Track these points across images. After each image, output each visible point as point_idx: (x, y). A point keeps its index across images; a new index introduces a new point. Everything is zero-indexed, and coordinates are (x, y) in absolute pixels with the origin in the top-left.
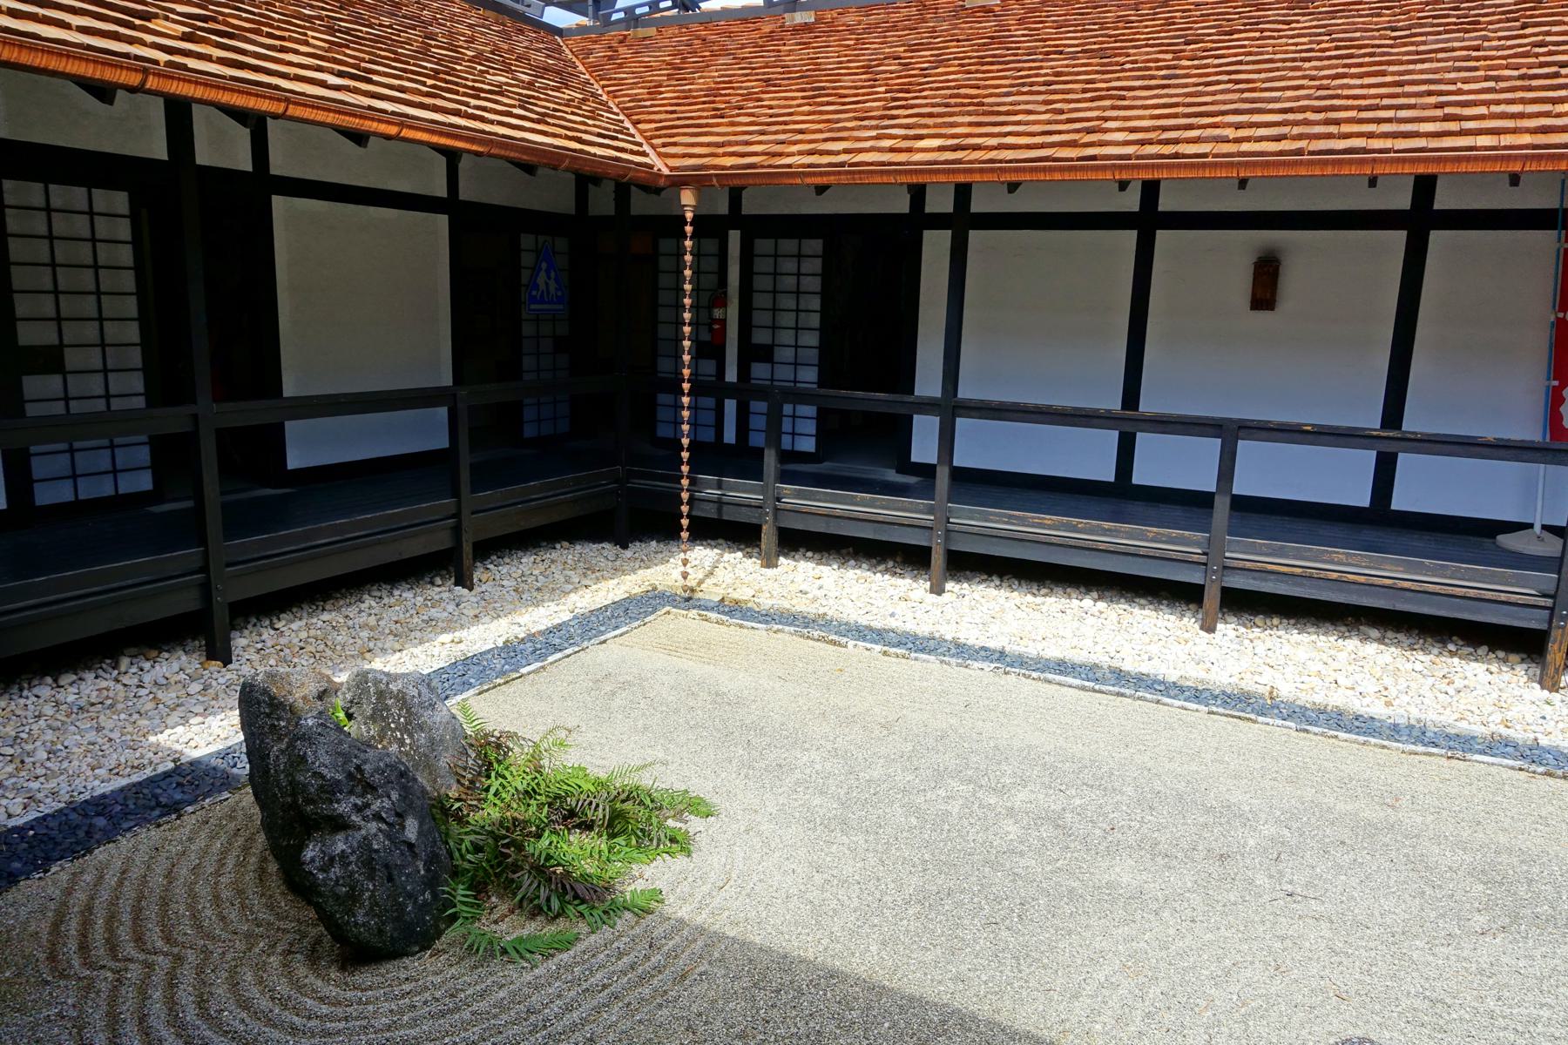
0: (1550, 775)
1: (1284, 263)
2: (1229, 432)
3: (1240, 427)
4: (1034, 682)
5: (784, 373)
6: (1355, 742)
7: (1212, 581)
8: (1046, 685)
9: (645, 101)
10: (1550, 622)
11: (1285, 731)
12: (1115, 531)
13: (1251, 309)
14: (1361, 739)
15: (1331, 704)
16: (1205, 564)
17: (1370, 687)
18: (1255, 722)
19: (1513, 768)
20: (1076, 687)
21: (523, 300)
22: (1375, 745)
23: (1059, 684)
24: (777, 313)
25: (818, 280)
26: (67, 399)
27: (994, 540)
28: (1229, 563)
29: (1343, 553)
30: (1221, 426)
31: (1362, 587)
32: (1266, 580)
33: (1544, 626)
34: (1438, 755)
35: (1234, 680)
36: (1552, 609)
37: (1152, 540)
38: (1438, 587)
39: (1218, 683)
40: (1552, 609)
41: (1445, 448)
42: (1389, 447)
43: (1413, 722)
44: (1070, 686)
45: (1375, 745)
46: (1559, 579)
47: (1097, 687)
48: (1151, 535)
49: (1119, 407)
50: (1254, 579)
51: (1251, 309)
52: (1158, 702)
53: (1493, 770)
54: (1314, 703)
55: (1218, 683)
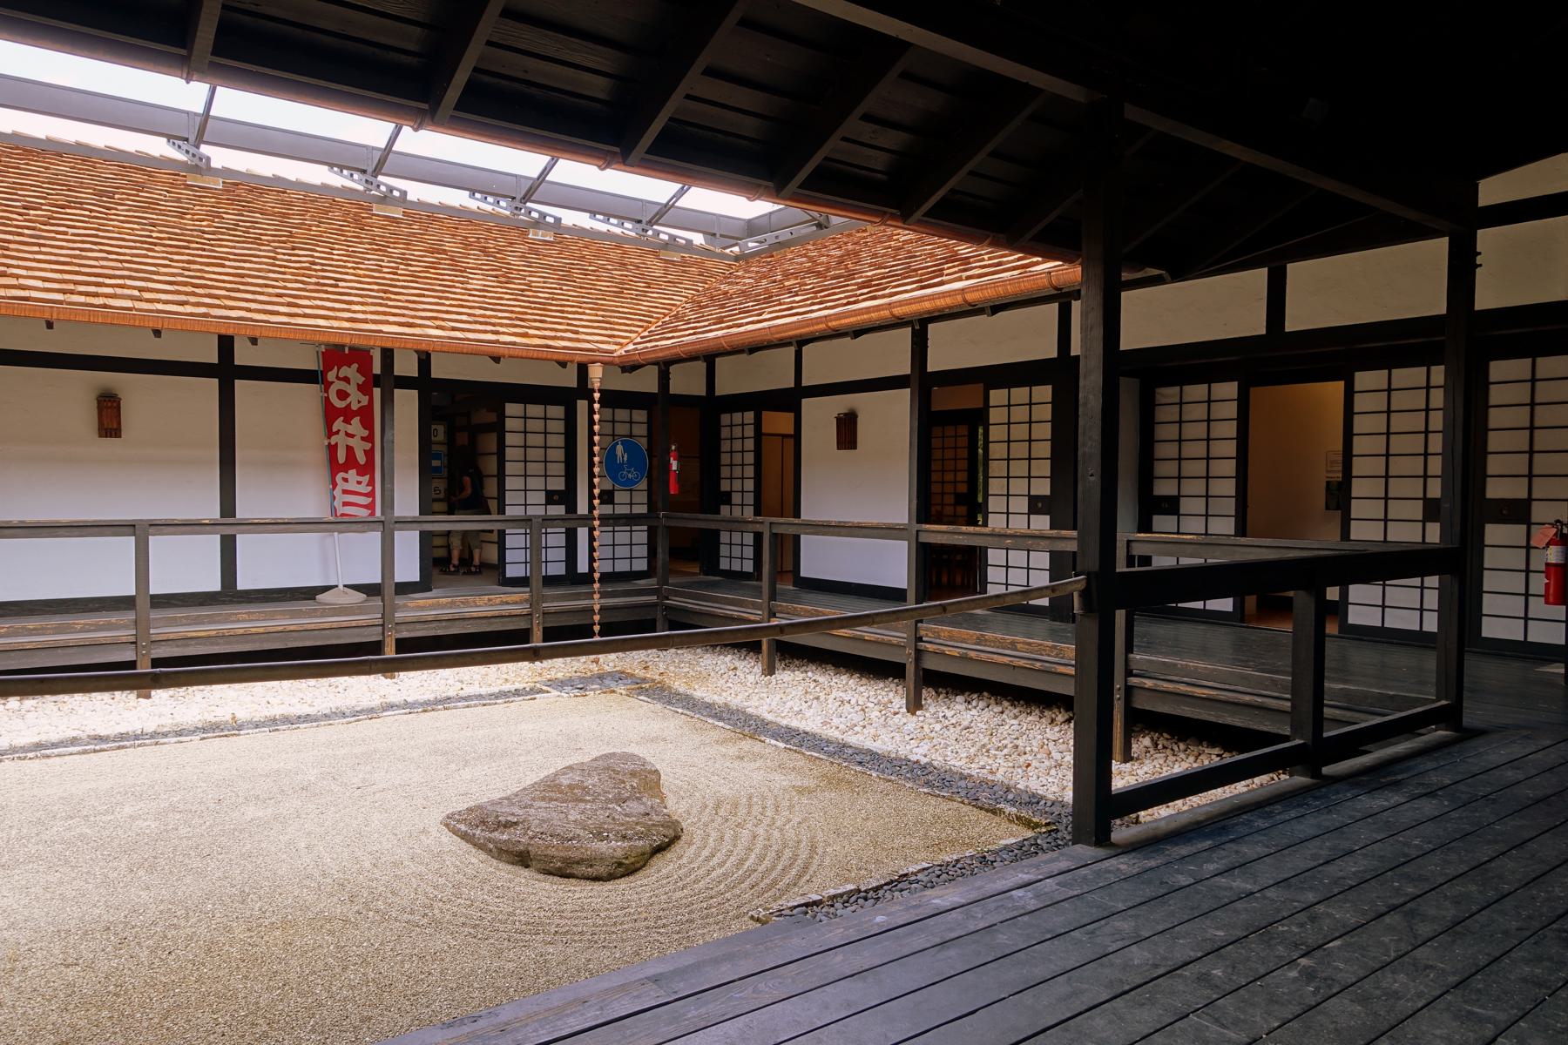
0: (425, 711)
1: (859, 415)
2: (139, 531)
3: (151, 525)
4: (31, 761)
5: (737, 512)
6: (312, 727)
7: (143, 655)
8: (47, 761)
9: (867, 271)
10: (383, 633)
11: (264, 734)
12: (42, 629)
13: (855, 448)
14: (314, 724)
15: (278, 714)
16: (135, 643)
17: (295, 701)
18: (239, 735)
19: (406, 714)
20: (79, 753)
21: (446, 458)
22: (325, 725)
23: (59, 755)
24: (1182, 480)
25: (966, 451)
26: (1007, 585)
27: (12, 654)
28: (154, 638)
29: (246, 613)
30: (134, 526)
31: (263, 636)
32: (187, 645)
33: (380, 638)
34: (363, 719)
35: (199, 717)
36: (383, 625)
37: (81, 631)
38: (313, 625)
39: (190, 723)
40: (383, 625)
41: (184, 528)
42: (228, 531)
43: (334, 710)
44: (71, 754)
45: (325, 725)
46: (384, 605)
47: (98, 748)
48: (79, 627)
49: (418, 514)
50: (177, 646)
51: (855, 448)
52: (157, 744)
53: (396, 717)
54: (266, 717)
55: (190, 723)
